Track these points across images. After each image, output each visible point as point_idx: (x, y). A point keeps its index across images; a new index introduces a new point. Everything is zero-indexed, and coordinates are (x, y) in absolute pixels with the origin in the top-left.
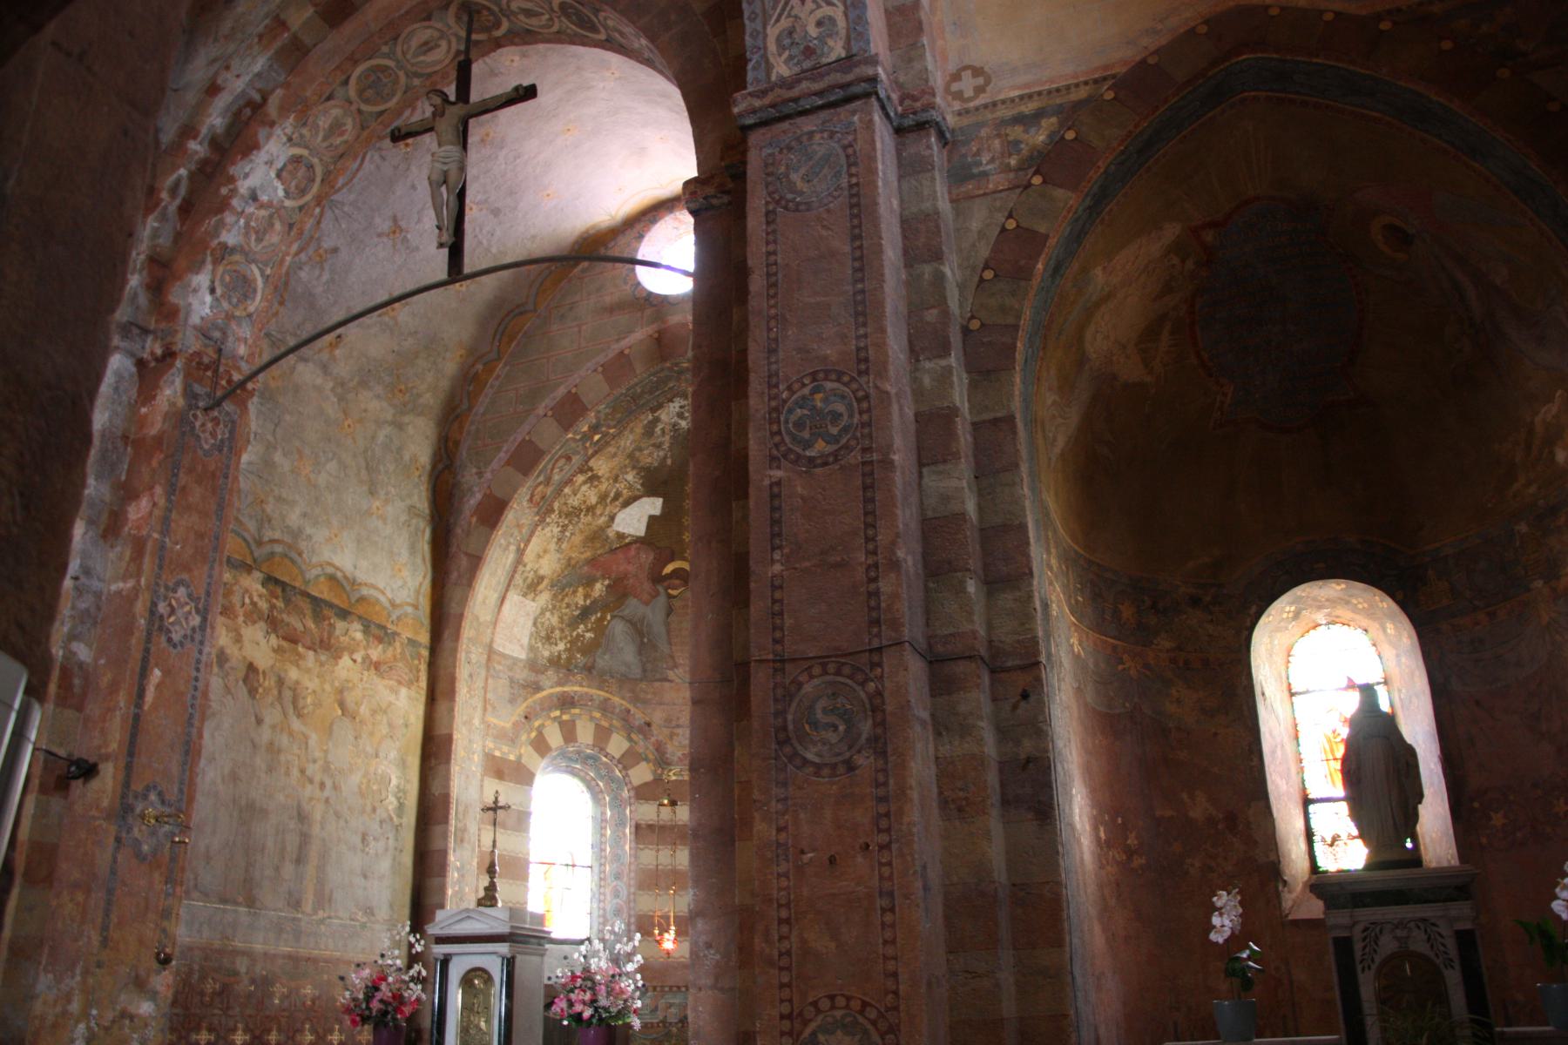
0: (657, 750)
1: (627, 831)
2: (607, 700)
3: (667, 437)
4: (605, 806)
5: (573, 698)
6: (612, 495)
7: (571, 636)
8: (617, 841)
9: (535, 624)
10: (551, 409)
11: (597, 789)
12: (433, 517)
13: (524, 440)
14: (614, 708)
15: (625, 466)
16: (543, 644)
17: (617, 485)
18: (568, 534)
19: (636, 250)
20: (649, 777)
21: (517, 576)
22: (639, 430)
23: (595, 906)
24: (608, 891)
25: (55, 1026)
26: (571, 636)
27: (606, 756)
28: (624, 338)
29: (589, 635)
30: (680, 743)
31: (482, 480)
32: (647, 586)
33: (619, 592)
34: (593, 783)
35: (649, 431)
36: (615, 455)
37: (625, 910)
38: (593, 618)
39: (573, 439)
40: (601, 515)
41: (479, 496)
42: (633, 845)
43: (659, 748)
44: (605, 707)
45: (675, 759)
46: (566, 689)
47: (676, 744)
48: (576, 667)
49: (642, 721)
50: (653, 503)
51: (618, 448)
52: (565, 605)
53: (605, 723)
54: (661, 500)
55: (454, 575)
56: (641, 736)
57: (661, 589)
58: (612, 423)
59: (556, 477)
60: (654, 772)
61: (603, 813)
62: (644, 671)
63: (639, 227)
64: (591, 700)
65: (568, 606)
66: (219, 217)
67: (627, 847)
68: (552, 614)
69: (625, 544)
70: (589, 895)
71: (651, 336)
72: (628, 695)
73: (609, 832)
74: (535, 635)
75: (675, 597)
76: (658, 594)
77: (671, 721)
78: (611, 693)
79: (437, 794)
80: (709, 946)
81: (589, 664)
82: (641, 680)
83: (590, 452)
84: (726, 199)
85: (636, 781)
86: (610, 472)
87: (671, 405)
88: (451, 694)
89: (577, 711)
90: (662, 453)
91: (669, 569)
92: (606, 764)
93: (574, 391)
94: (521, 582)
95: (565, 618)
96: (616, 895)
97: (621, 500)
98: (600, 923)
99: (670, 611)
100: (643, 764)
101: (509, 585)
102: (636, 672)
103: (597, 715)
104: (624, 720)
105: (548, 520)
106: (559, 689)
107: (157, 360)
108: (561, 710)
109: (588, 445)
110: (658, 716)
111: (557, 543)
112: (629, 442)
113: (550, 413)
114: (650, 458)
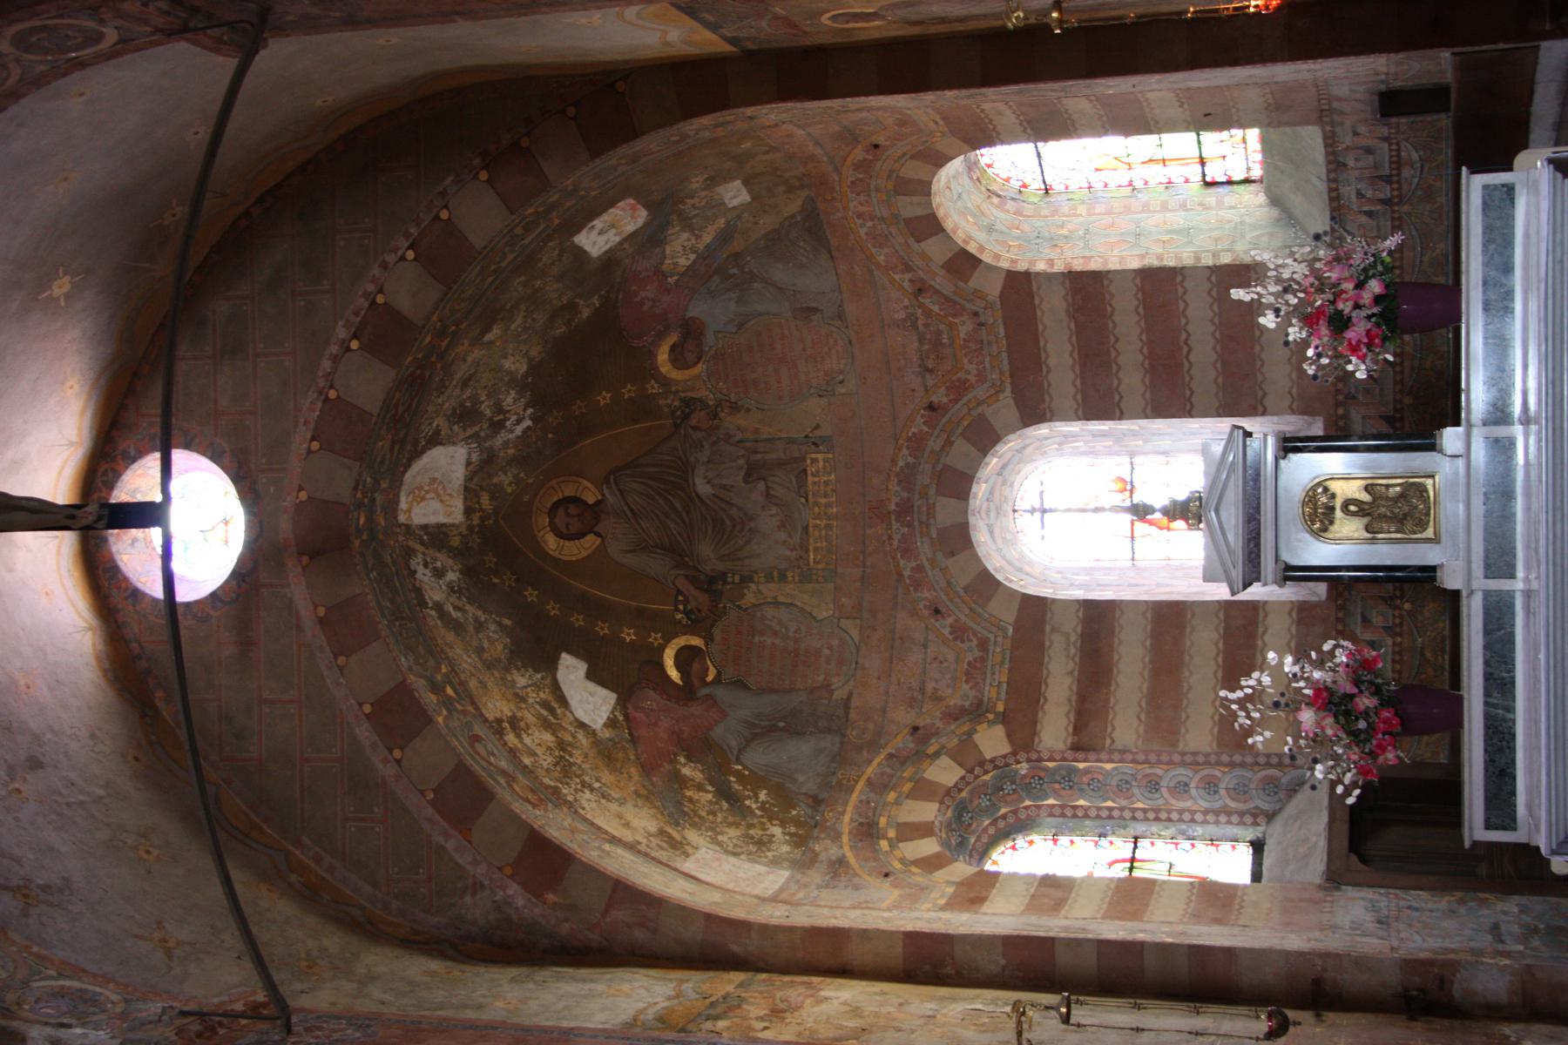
0: (956, 719)
1: (1081, 766)
2: (869, 782)
3: (468, 607)
4: (1039, 807)
5: (861, 824)
6: (545, 713)
7: (761, 817)
8: (1097, 786)
9: (734, 854)
10: (391, 751)
11: (1011, 820)
12: (532, 965)
13: (433, 803)
14: (883, 774)
15: (503, 679)
16: (769, 850)
17: (531, 700)
18: (597, 785)
20: (999, 731)
21: (653, 854)
22: (450, 636)
23: (1199, 830)
26: (761, 817)
27: (960, 790)
29: (763, 796)
30: (948, 686)
31: (486, 883)
32: (696, 709)
33: (700, 747)
34: (1001, 824)
35: (457, 627)
36: (483, 684)
37: (1206, 772)
38: (737, 786)
39: (446, 718)
40: (574, 737)
41: (513, 889)
42: (1104, 756)
43: (953, 716)
44: (880, 786)
45: (972, 693)
46: (846, 831)
47: (950, 691)
48: (812, 818)
49: (910, 738)
50: (567, 667)
51: (472, 675)
52: (711, 817)
54: (564, 655)
55: (640, 935)
56: (933, 741)
58: (431, 663)
59: (503, 764)
60: (991, 723)
62: (829, 730)
63: (116, 599)
64: (868, 802)
65: (713, 813)
67: (1108, 766)
68: (722, 833)
69: (624, 718)
71: (304, 568)
72: (865, 753)
74: (754, 858)
75: (719, 674)
77: (912, 698)
78: (859, 777)
79: (1003, 962)
81: (810, 801)
82: (844, 736)
83: (470, 708)
85: (1004, 748)
86: (509, 701)
87: (419, 576)
88: (837, 935)
89: (883, 821)
91: (674, 674)
92: (972, 793)
93: (367, 709)
94: (664, 853)
95: (731, 819)
96: (1181, 789)
97: (555, 705)
98: (1229, 822)
99: (740, 684)
101: (668, 866)
102: (830, 742)
103: (892, 796)
104: (903, 763)
105: (570, 798)
106: (845, 839)
108: (878, 838)
109: (460, 707)
110: (904, 716)
111: (609, 800)
112: (465, 657)
113: (397, 753)
114: (498, 646)
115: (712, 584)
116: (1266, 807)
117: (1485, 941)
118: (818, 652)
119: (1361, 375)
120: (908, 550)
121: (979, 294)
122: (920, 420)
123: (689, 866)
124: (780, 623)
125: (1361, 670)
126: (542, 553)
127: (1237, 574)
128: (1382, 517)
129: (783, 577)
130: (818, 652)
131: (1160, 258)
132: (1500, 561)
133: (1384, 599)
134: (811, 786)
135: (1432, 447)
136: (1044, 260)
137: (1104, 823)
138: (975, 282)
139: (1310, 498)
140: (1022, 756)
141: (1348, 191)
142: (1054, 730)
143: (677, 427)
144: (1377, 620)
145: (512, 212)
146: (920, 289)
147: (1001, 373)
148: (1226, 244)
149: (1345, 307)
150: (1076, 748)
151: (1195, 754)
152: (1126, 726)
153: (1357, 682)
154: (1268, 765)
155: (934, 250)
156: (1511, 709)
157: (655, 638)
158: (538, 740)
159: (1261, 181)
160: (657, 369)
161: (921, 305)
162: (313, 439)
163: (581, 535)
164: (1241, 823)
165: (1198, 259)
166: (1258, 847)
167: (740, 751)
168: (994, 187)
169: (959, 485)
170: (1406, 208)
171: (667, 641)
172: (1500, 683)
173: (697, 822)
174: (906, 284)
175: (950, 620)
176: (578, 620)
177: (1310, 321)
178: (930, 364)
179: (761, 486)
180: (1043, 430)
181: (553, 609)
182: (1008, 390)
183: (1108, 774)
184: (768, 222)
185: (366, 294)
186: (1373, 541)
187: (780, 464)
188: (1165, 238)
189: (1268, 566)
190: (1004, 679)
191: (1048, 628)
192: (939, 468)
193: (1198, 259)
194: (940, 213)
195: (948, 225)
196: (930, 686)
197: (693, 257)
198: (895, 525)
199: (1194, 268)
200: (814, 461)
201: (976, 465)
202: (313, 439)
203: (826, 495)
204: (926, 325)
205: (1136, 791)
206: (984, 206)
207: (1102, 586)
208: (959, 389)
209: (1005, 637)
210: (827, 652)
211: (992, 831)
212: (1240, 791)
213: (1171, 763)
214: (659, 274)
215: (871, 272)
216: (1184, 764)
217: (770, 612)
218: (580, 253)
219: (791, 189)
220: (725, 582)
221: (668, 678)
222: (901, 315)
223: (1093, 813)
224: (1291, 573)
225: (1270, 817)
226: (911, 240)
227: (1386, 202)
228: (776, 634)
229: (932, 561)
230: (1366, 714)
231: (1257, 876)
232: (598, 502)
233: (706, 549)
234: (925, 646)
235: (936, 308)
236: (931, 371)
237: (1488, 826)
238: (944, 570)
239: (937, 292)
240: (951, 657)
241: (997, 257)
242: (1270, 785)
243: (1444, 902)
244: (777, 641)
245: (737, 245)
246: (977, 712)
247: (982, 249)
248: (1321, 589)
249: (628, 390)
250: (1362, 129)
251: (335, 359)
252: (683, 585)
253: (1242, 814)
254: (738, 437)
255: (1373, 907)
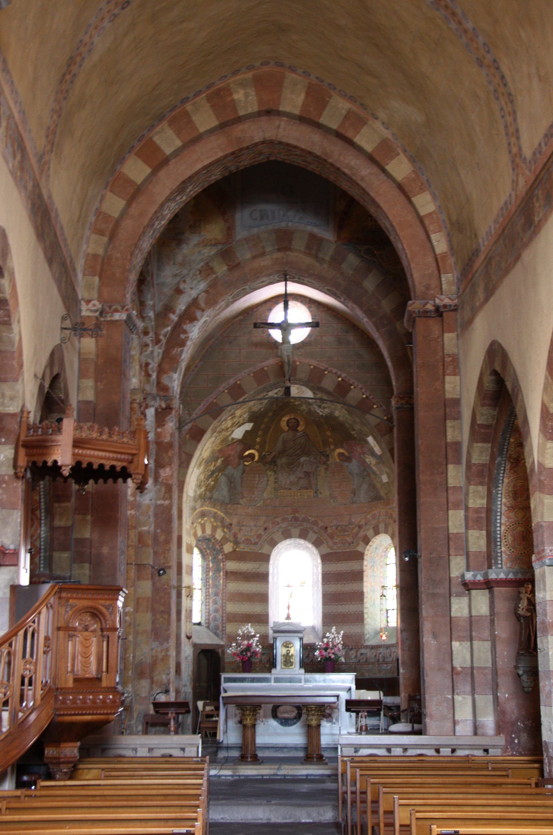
1: (221, 574)
2: (216, 513)
8: (215, 579)
13: (212, 402)
19: (267, 316)
20: (231, 550)
23: (204, 607)
24: (211, 601)
25: (163, 659)
28: (264, 361)
29: (212, 483)
33: (226, 463)
34: (204, 551)
42: (225, 580)
43: (235, 536)
44: (215, 516)
53: (215, 524)
57: (242, 462)
61: (208, 565)
62: (231, 499)
63: (269, 304)
66: (182, 348)
67: (221, 581)
70: (200, 603)
71: (277, 363)
73: (211, 574)
76: (240, 464)
80: (407, 639)
84: (408, 406)
89: (206, 519)
90: (261, 406)
91: (247, 453)
93: (238, 382)
96: (215, 602)
98: (206, 616)
99: (244, 472)
100: (229, 543)
102: (227, 500)
103: (212, 520)
106: (201, 509)
107: (162, 409)
110: (235, 521)
113: (226, 391)
115: (274, 462)
116: (211, 626)
117: (184, 683)
118: (253, 494)
119: (316, 654)
120: (284, 520)
121: (358, 544)
122: (322, 524)
123: (195, 469)
124: (262, 482)
125: (255, 653)
126: (283, 416)
127: (275, 629)
128: (286, 658)
129: (276, 482)
130: (253, 494)
131: (367, 597)
132: (277, 680)
133: (269, 659)
134: (215, 496)
135: (300, 667)
136: (367, 563)
137: (205, 581)
138: (361, 543)
139: (290, 643)
140: (224, 557)
141: (381, 650)
142: (231, 566)
143: (321, 452)
144: (264, 657)
145: (375, 426)
146: (360, 527)
147: (336, 549)
148: (370, 616)
149: (329, 650)
150: (227, 572)
151: (225, 606)
152: (234, 586)
153: (253, 652)
154: (223, 627)
155: (370, 532)
156: (248, 682)
157: (257, 447)
158: (229, 423)
159: (388, 626)
160: (337, 448)
161: (356, 527)
162: (314, 366)
163: (288, 426)
164: (206, 619)
165: (366, 608)
166: (199, 624)
167: (225, 474)
168: (388, 550)
169: (303, 535)
170: (377, 665)
171: (257, 450)
172: (253, 680)
173: (205, 468)
174: (361, 523)
175: (263, 533)
176: (263, 426)
177: (327, 644)
178: (339, 528)
179: (303, 476)
180: (319, 561)
181: (266, 420)
182: (331, 551)
183: (219, 581)
184: (378, 485)
185: (354, 383)
186: (282, 656)
187: (310, 482)
188: (373, 599)
189: (276, 635)
190: (246, 550)
191: (261, 563)
192: (309, 530)
193: (366, 608)
194: (380, 535)
195: (377, 537)
196: (243, 528)
197: (369, 463)
198: (291, 516)
199: (363, 607)
200: (311, 492)
201: (309, 541)
202: (314, 366)
203: (301, 495)
204: (350, 528)
205: (214, 589)
206: (383, 547)
207: (273, 578)
208: (331, 537)
209: (258, 550)
210: (253, 496)
211: (202, 548)
212: (215, 619)
213: (223, 599)
214: (364, 453)
215: (365, 513)
216: (222, 603)
217: (265, 479)
218: (368, 436)
219: (386, 494)
220: (274, 466)
221: (245, 452)
222: (353, 520)
223: (208, 577)
224: (275, 639)
225: (208, 627)
226: (373, 526)
227: (378, 660)
228: (259, 481)
229: (280, 527)
230: (246, 654)
231: (195, 624)
232: (298, 431)
233: (284, 460)
234: (255, 526)
235: (354, 531)
236: (337, 528)
237: (225, 678)
238: (278, 531)
239: (359, 532)
240: (252, 534)
241: (368, 550)
242: (217, 627)
243: (190, 673)
244: (257, 482)
245: (372, 476)
246: (236, 542)
247: (371, 546)
248: (272, 642)
249: (331, 440)
250: (395, 654)
251: (336, 373)
252: (273, 454)
253: (208, 619)
254: (318, 470)
255: (189, 656)
